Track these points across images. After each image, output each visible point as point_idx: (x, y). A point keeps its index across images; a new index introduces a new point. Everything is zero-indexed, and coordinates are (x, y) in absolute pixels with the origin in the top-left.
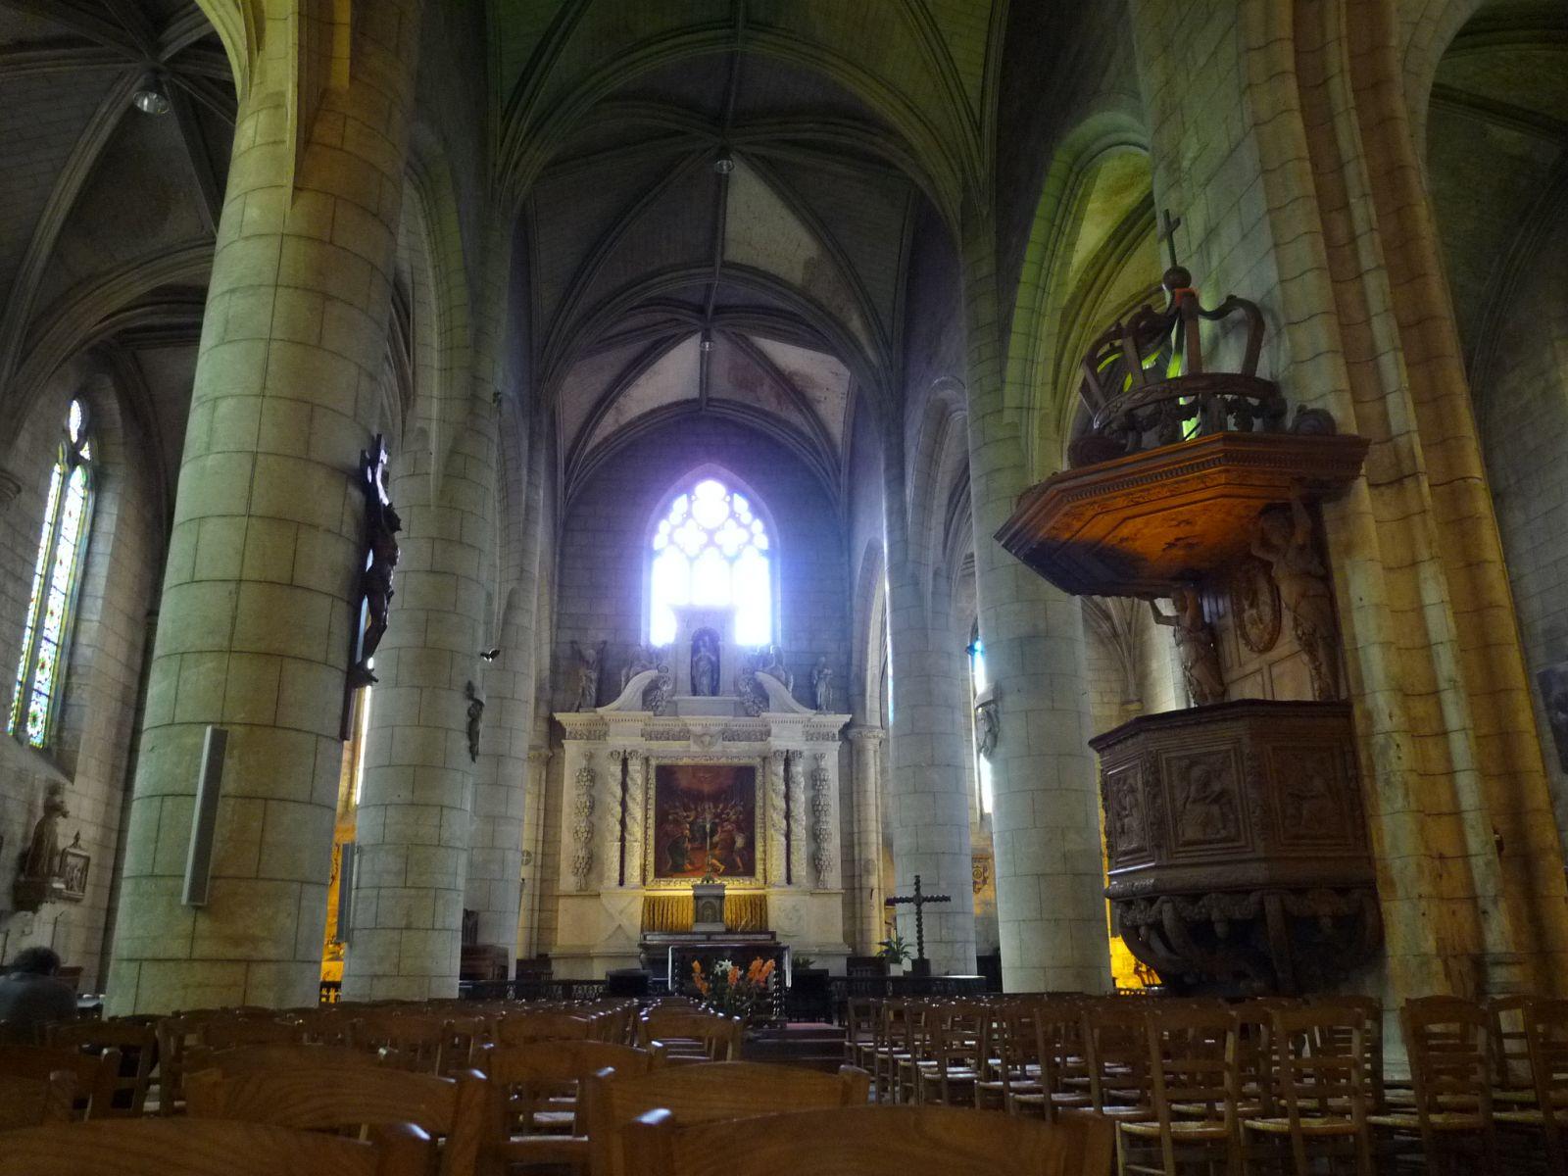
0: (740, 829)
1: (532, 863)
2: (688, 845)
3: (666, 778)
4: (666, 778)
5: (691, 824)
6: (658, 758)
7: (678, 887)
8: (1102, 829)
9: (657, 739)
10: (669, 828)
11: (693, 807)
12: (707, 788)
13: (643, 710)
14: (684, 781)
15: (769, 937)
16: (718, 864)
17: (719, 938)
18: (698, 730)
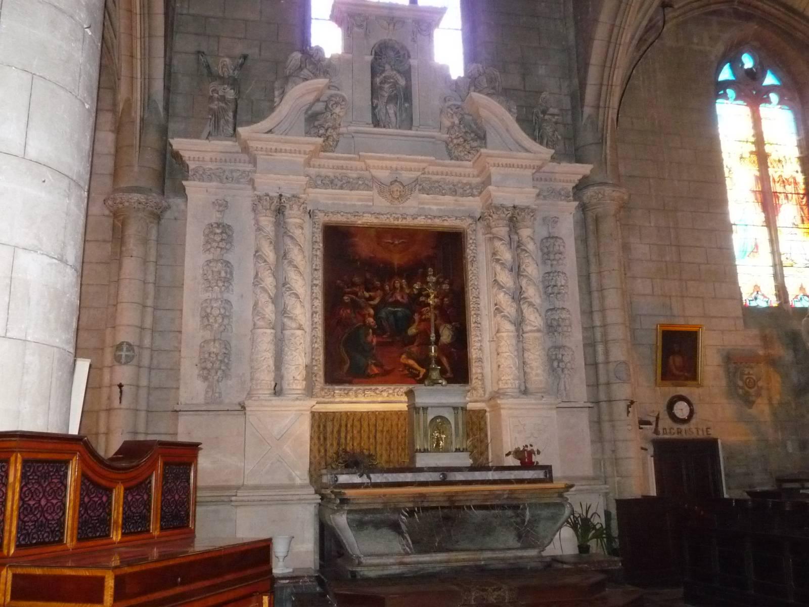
0: (447, 319)
1: (135, 361)
2: (373, 339)
3: (338, 240)
4: (338, 240)
5: (375, 308)
6: (326, 213)
7: (362, 399)
8: (393, 309)
9: (325, 186)
10: (345, 313)
11: (378, 283)
12: (397, 259)
13: (307, 133)
14: (364, 248)
15: (540, 474)
16: (416, 366)
17: (459, 476)
18: (383, 175)
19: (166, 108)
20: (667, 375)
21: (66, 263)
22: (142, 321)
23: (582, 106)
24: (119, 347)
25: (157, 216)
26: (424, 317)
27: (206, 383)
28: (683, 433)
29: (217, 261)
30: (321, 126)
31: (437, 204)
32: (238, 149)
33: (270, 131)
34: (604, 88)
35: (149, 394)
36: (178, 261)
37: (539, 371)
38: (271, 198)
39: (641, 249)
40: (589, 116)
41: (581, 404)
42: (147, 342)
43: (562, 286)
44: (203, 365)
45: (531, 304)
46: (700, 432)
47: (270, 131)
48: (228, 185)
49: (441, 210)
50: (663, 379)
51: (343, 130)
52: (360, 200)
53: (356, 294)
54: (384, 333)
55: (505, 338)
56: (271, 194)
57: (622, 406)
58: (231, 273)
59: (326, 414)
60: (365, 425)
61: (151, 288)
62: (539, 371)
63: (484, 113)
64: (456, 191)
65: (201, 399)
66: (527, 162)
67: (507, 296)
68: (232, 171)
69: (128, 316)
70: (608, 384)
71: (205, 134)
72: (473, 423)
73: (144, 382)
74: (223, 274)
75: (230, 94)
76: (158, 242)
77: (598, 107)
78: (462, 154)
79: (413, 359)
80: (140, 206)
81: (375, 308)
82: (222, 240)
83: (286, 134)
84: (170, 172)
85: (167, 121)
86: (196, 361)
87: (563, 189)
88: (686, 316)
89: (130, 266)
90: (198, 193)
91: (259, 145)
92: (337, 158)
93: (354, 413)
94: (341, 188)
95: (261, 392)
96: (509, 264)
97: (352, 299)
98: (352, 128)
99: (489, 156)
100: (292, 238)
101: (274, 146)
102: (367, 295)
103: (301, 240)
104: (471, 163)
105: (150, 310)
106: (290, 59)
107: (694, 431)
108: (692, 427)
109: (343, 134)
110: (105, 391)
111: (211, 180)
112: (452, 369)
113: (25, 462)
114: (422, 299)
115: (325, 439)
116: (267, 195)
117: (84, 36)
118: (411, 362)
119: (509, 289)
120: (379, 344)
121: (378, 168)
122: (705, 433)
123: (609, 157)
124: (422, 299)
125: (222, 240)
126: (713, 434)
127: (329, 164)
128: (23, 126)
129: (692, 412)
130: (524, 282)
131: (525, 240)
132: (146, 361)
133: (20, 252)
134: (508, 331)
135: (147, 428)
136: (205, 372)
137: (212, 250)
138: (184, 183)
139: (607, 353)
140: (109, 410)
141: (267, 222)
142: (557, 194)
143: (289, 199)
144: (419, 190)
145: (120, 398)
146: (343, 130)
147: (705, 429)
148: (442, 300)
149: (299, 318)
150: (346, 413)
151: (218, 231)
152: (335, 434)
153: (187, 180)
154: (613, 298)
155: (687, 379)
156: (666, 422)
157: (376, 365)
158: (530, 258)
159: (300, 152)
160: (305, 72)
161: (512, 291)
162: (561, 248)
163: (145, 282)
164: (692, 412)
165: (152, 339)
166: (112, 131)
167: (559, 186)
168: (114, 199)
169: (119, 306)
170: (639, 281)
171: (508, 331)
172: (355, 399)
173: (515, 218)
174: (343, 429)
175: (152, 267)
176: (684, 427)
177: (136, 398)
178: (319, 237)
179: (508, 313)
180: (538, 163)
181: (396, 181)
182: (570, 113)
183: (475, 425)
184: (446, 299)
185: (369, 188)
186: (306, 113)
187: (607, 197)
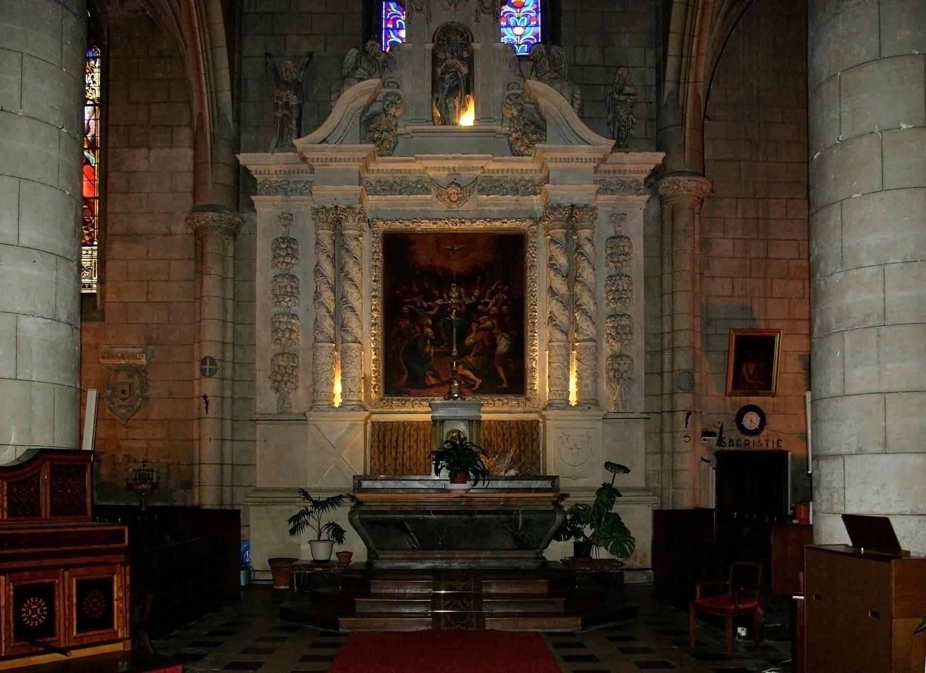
0: (504, 328)
1: (218, 375)
2: (430, 349)
3: (397, 248)
4: (397, 248)
5: (433, 317)
7: (419, 410)
11: (436, 293)
12: (456, 266)
14: (423, 256)
15: (547, 484)
16: (472, 376)
19: (237, 120)
20: (740, 384)
21: (59, 321)
22: (224, 337)
23: (664, 81)
24: (203, 362)
25: (233, 232)
26: (481, 326)
27: (278, 395)
28: (751, 445)
29: (283, 276)
30: (376, 130)
31: (497, 205)
32: (298, 160)
33: (324, 141)
34: (684, 60)
35: (233, 404)
36: (252, 279)
37: (588, 382)
38: (328, 211)
39: (724, 246)
40: (671, 94)
41: (637, 415)
42: (229, 356)
43: (624, 290)
44: (274, 378)
45: (584, 312)
46: (770, 445)
47: (324, 141)
48: (293, 197)
49: (501, 211)
50: (735, 387)
51: (400, 130)
52: (418, 205)
53: (414, 303)
54: (442, 343)
55: (556, 348)
56: (327, 206)
57: (681, 416)
58: (297, 288)
59: (385, 424)
60: (421, 433)
61: (230, 304)
62: (588, 382)
63: (542, 102)
64: (517, 190)
65: (274, 409)
66: (588, 156)
67: (559, 304)
68: (295, 182)
69: (211, 331)
70: (672, 394)
71: (273, 144)
72: (526, 434)
73: (228, 393)
74: (289, 289)
75: (294, 100)
76: (235, 258)
77: (679, 83)
78: (522, 149)
79: (470, 370)
80: (215, 224)
81: (433, 317)
82: (287, 254)
83: (341, 143)
84: (243, 186)
85: (239, 133)
86: (269, 374)
87: (633, 182)
88: (769, 316)
89: (211, 284)
90: (265, 207)
91: (315, 155)
92: (395, 161)
93: (411, 423)
94: (401, 193)
95: (320, 403)
96: (564, 270)
97: (410, 309)
98: (410, 128)
99: (544, 151)
100: (348, 250)
101: (328, 155)
102: (425, 304)
103: (357, 253)
104: (531, 158)
105: (230, 325)
106: (348, 57)
107: (764, 443)
108: (761, 438)
109: (401, 134)
110: (196, 401)
111: (276, 194)
112: (507, 380)
113: (52, 467)
114: (480, 307)
115: (384, 447)
116: (324, 207)
117: (60, 136)
118: (468, 372)
119: (562, 296)
120: (435, 354)
121: (435, 168)
122: (776, 445)
123: (687, 142)
124: (480, 307)
125: (287, 254)
126: (784, 446)
127: (386, 167)
128: (15, 222)
129: (763, 423)
130: (578, 288)
131: (584, 242)
132: (229, 373)
133: (21, 317)
134: (558, 341)
135: (233, 434)
136: (276, 384)
137: (279, 265)
138: (253, 198)
139: (673, 359)
140: (200, 418)
141: (326, 235)
142: (625, 187)
143: (344, 210)
144: (479, 191)
145: (206, 408)
146: (400, 130)
147: (776, 441)
148: (500, 308)
149: (355, 330)
150: (403, 422)
151: (284, 246)
152: (394, 443)
153: (255, 194)
154: (682, 302)
155: (761, 387)
156: (736, 434)
157: (433, 376)
158: (586, 262)
159: (354, 160)
160: (360, 72)
161: (565, 297)
162: (626, 248)
163: (224, 299)
164: (763, 423)
165: (234, 352)
166: (190, 147)
167: (629, 177)
168: (194, 218)
169: (204, 323)
170: (719, 280)
171: (558, 341)
172: (412, 410)
173: (572, 217)
174: (401, 438)
175: (230, 282)
176: (752, 439)
177: (222, 408)
178: (379, 247)
179: (561, 322)
180: (600, 156)
181: (453, 183)
182: (654, 89)
183: (526, 438)
184: (504, 307)
185: (428, 191)
186: (361, 117)
187: (685, 187)
